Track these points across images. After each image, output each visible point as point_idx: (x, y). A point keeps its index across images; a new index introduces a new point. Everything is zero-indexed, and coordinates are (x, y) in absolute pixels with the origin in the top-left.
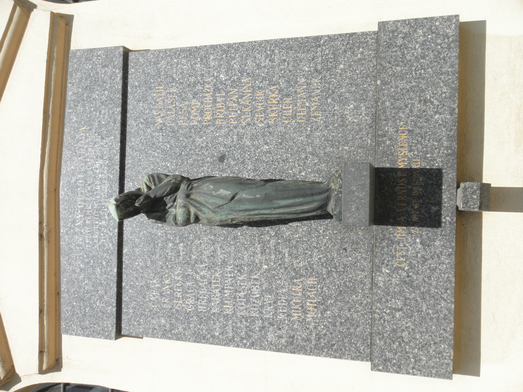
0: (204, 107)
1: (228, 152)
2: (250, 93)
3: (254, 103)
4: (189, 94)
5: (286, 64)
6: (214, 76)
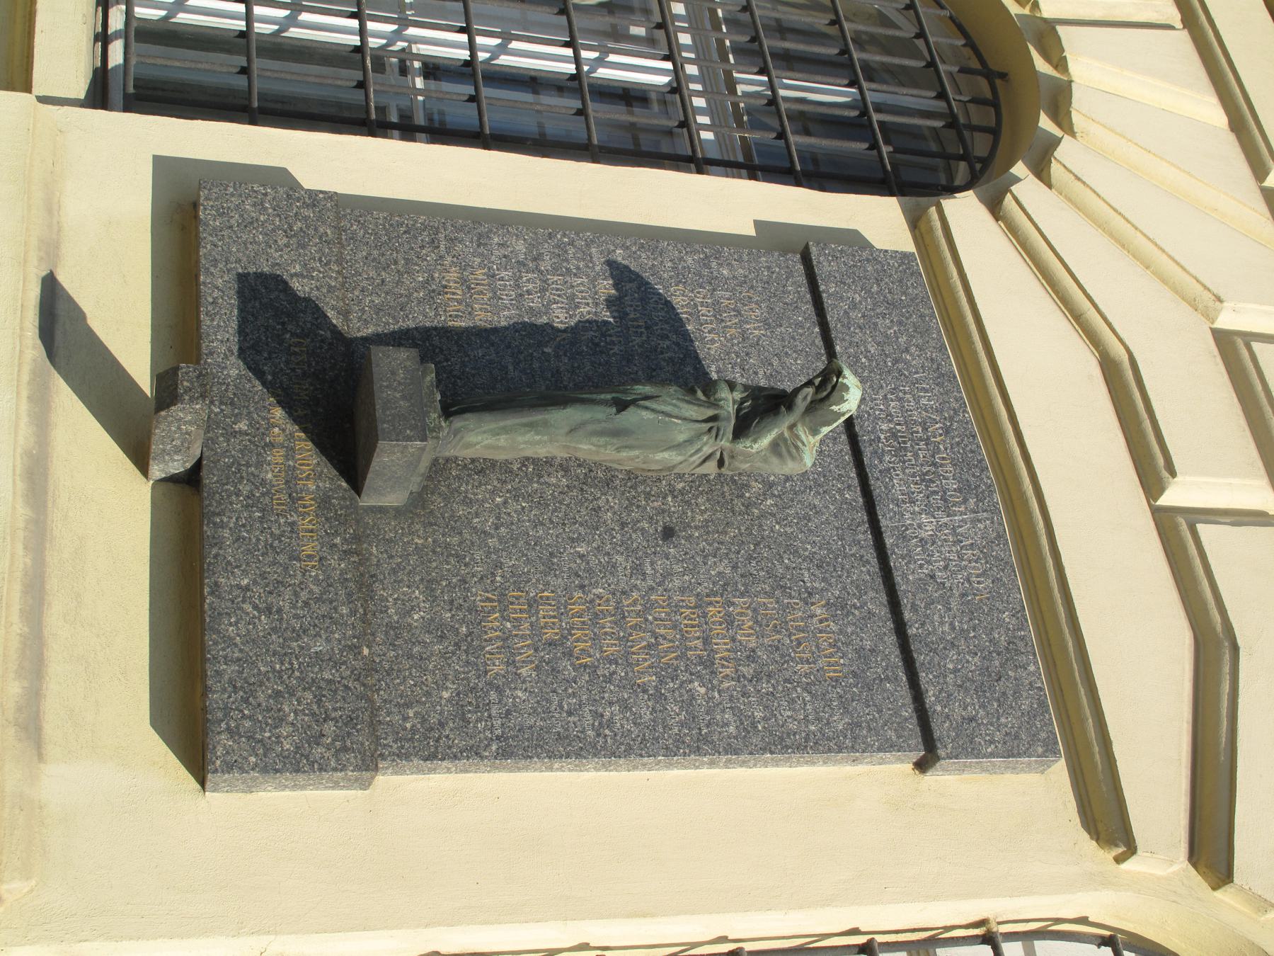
6: (719, 692)
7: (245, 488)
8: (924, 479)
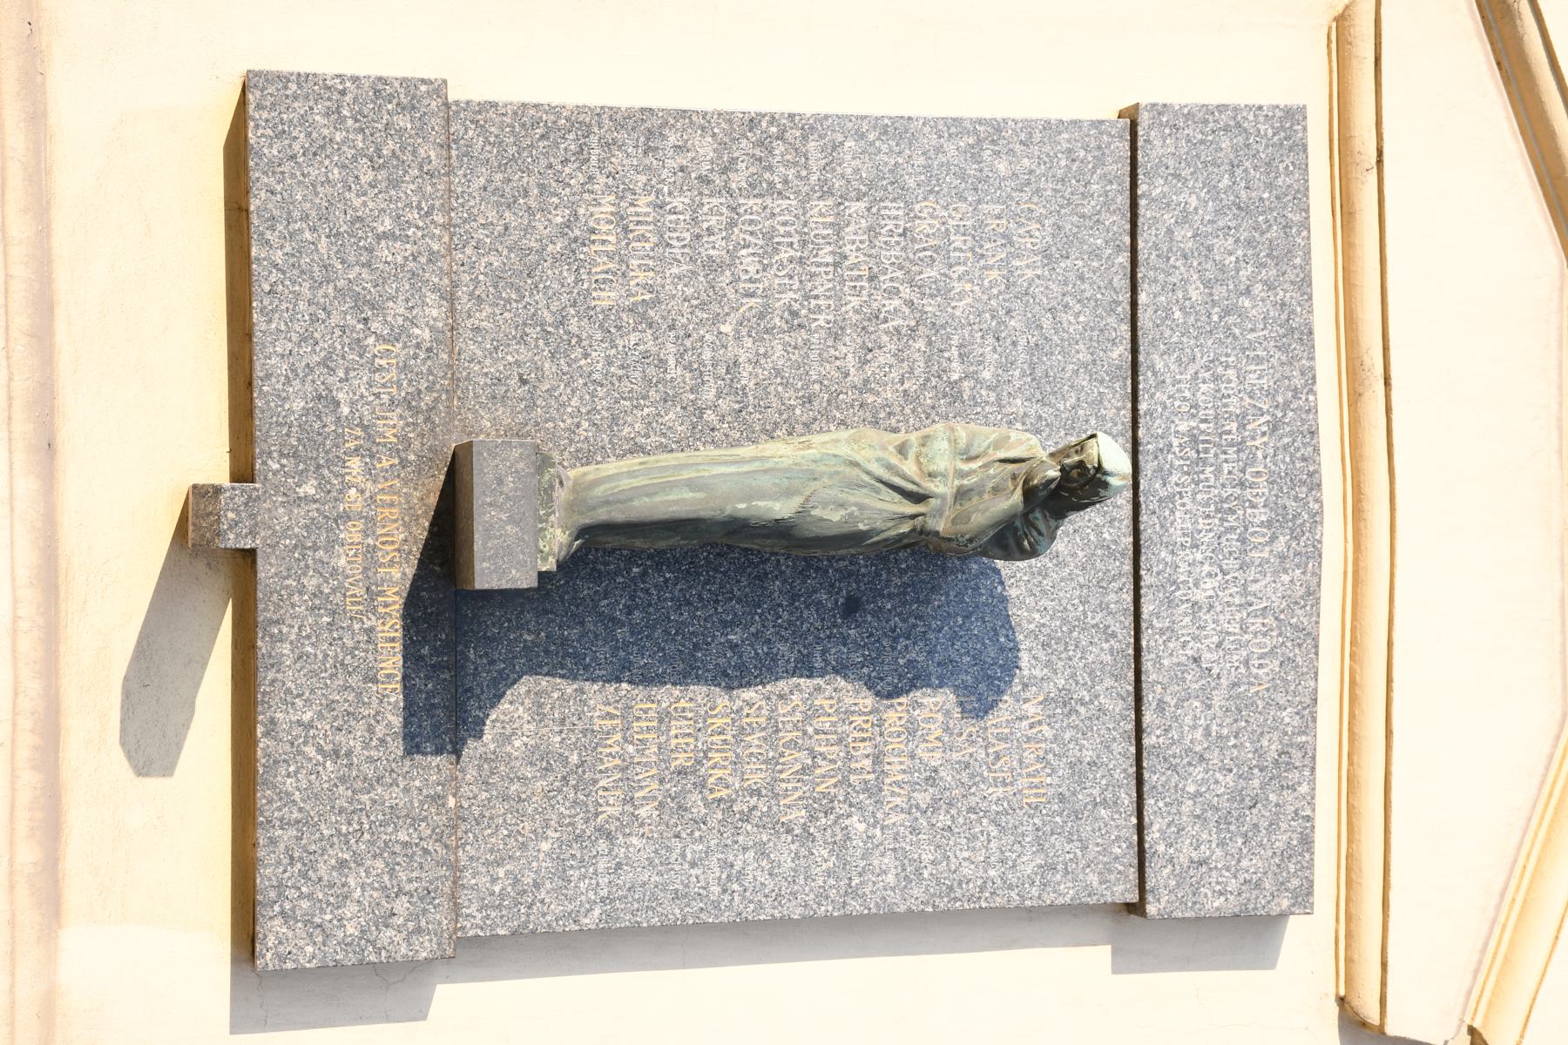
3: (771, 754)
5: (689, 856)
7: (311, 582)
8: (1223, 509)
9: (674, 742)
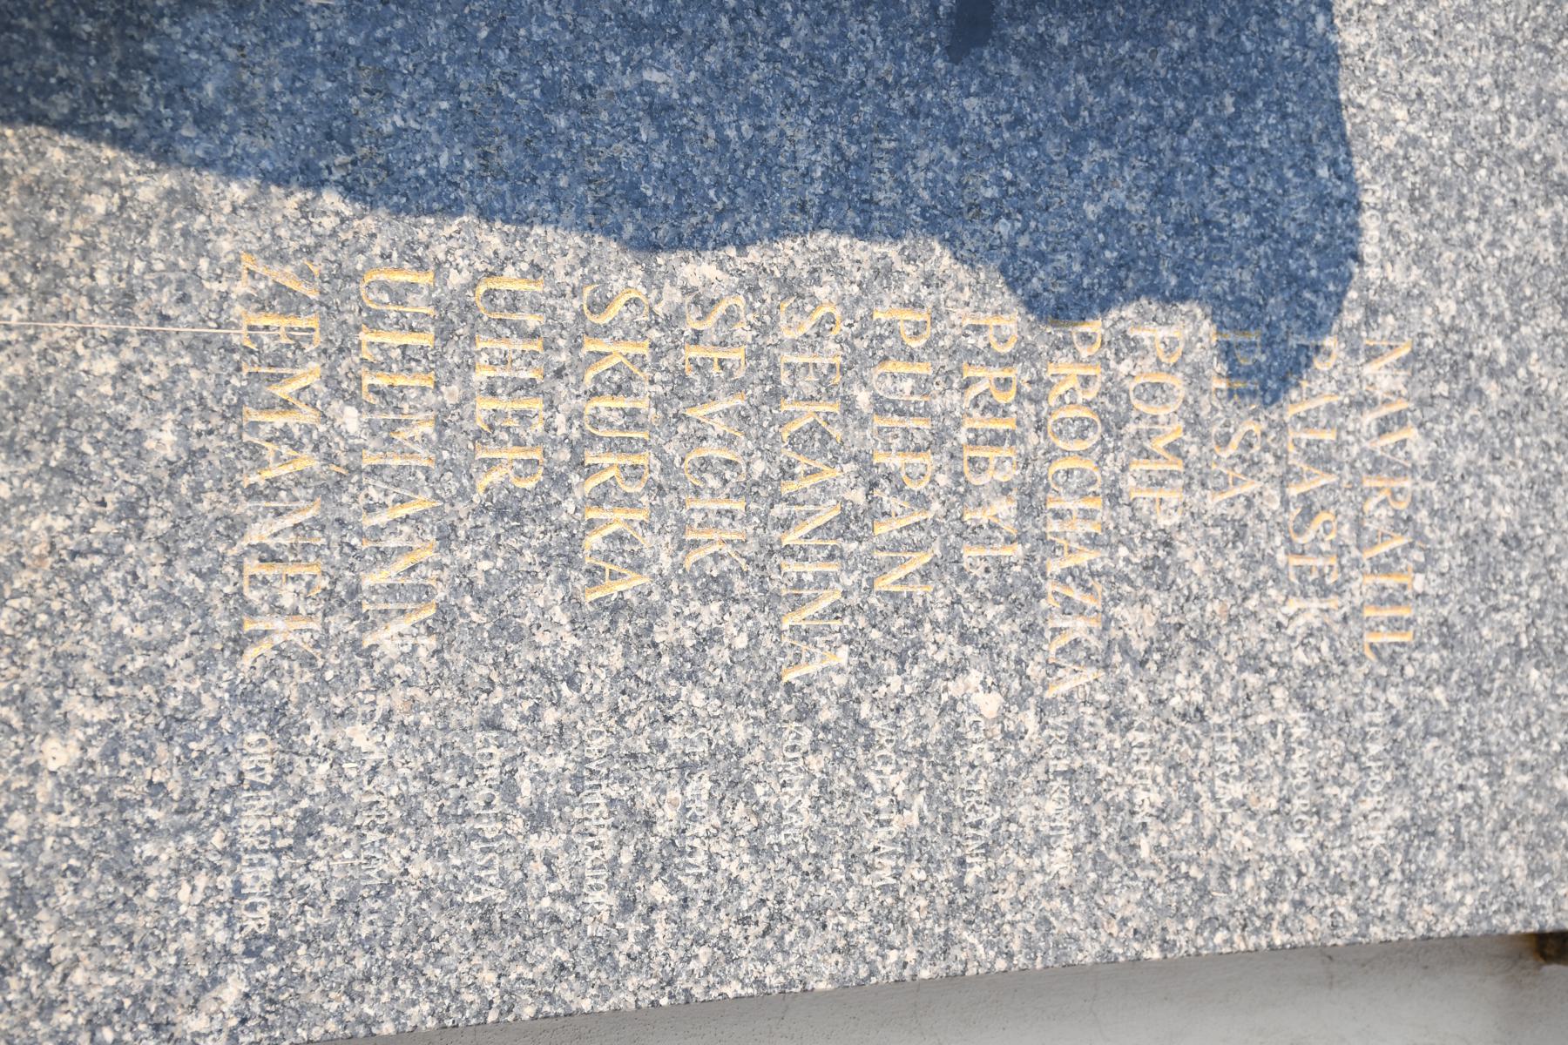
0: (1100, 462)
1: (929, 79)
2: (789, 552)
3: (759, 467)
4: (1198, 567)
5: (526, 788)
9: (485, 405)
